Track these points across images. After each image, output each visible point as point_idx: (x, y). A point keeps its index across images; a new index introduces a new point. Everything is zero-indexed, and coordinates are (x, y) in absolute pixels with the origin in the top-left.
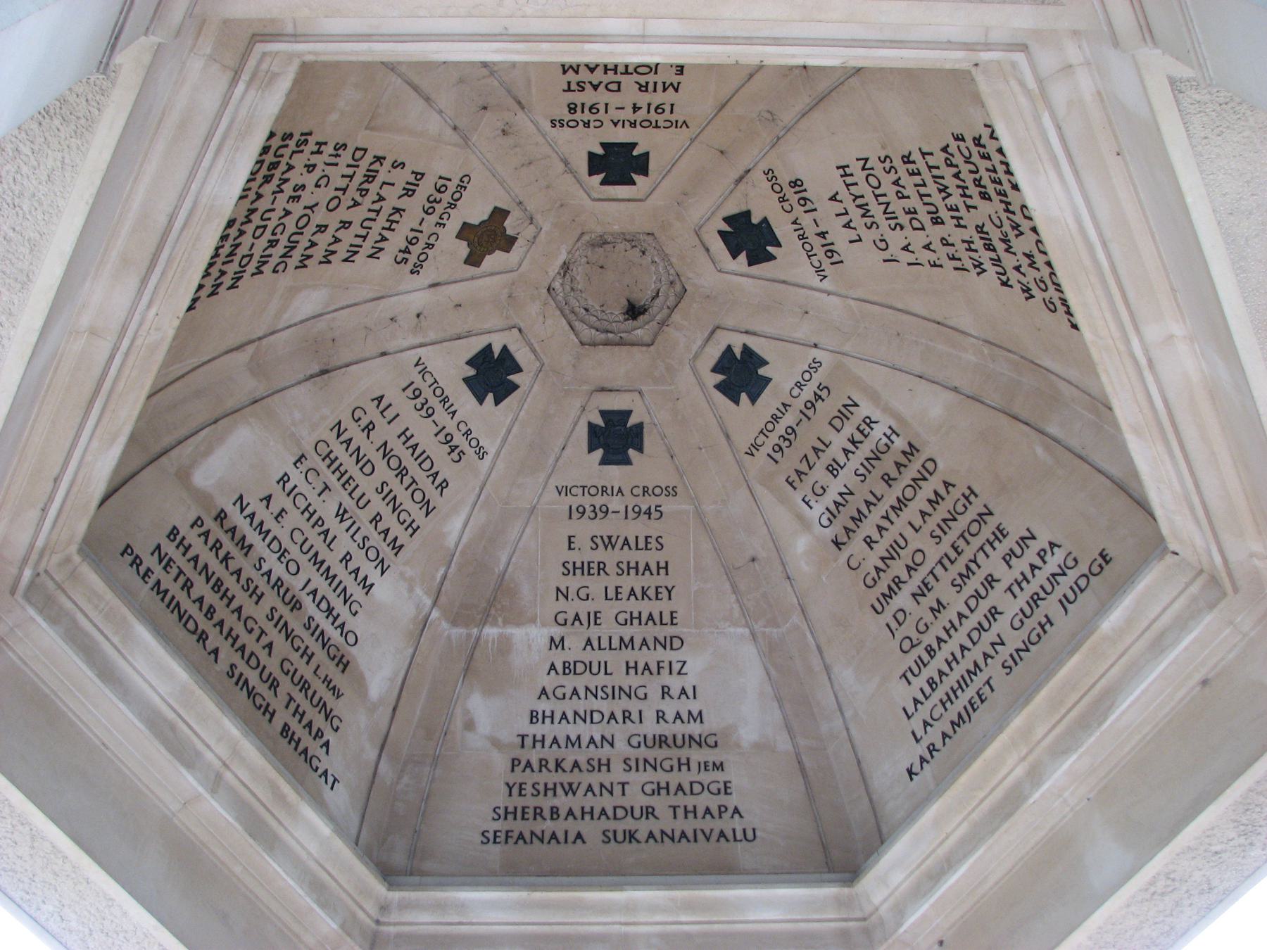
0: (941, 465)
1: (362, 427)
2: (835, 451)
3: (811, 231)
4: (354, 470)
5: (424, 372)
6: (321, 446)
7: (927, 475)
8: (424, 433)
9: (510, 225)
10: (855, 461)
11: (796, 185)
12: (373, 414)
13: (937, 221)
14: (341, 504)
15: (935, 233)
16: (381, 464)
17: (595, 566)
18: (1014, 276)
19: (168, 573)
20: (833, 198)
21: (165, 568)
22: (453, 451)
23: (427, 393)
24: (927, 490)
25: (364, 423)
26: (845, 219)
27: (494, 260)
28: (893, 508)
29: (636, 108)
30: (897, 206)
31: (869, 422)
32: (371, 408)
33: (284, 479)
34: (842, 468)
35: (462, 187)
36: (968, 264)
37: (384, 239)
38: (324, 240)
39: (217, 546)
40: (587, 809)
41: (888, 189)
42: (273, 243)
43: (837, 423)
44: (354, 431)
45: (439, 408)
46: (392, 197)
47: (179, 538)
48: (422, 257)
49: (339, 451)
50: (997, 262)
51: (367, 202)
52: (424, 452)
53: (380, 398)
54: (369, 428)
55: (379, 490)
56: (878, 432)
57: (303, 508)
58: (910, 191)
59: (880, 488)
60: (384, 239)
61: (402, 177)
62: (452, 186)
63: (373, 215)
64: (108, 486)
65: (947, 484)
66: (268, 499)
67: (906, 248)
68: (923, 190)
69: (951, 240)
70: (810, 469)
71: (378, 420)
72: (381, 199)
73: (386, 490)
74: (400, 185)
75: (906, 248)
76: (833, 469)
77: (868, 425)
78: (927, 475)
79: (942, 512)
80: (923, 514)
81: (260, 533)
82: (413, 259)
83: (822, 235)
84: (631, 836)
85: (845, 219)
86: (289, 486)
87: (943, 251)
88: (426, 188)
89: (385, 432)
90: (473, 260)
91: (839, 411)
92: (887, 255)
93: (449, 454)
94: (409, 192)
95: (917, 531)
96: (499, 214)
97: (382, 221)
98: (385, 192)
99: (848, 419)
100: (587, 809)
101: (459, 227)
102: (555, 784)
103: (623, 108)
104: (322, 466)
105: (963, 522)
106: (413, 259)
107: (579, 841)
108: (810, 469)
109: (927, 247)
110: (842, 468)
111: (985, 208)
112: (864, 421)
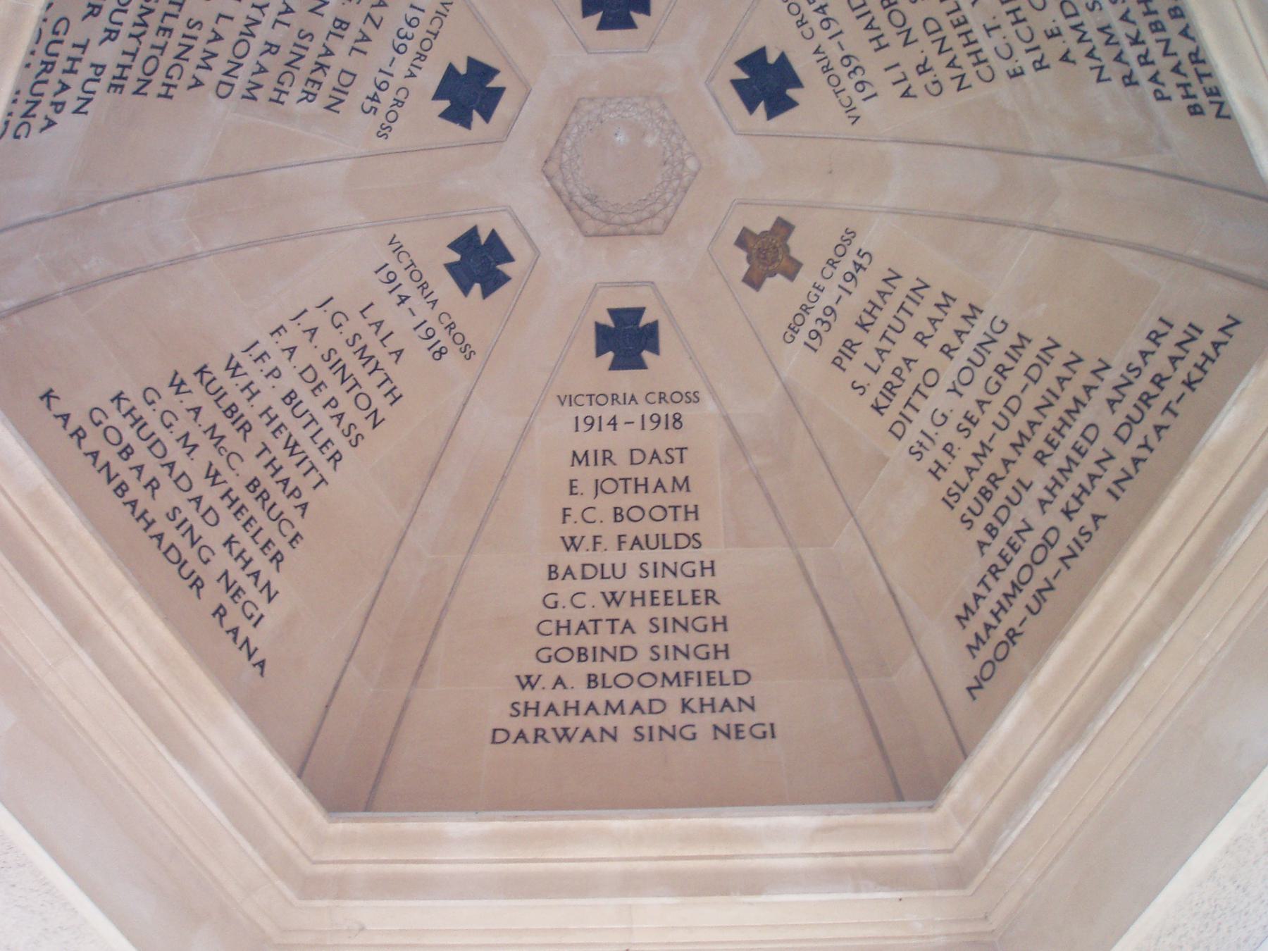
0: (212, 97)
1: (949, 458)
2: (341, 46)
3: (416, 301)
4: (952, 35)
5: (850, 108)
6: (988, 76)
7: (226, 79)
8: (856, 39)
9: (740, 263)
10: (315, 48)
11: (440, 352)
12: (917, 83)
13: (290, 398)
14: (211, 465)
15: (290, 380)
16: (915, 22)
17: (702, 594)
18: (199, 396)
19: (157, 34)
20: (399, 353)
21: (112, 85)
22: (372, 99)
23: (849, 84)
24: (219, 65)
25: (928, 77)
26: (384, 331)
27: (762, 223)
28: (257, 22)
29: (613, 423)
30: (334, 389)
31: (309, 96)
32: (917, 89)
33: (1040, 65)
34: (330, 33)
35: (793, 329)
36: (246, 362)
37: (882, 294)
38: (945, 335)
39: (1144, 60)
40: (572, 704)
41: (346, 404)
42: (1001, 370)
43: (346, 79)
44: (945, 74)
45: (835, 63)
46: (870, 341)
47: (259, 490)
48: (840, 250)
49: (965, 61)
50: (219, 395)
51: (894, 360)
52: (858, 17)
53: (905, 94)
54: (923, 69)
55: (326, 358)
56: (296, 92)
57: (554, 630)
58: (324, 416)
59: (279, 35)
60: (882, 294)
61: (855, 368)
62: (803, 336)
63: (891, 334)
64: (290, 771)
65: (198, 83)
66: (1065, 58)
67: (313, 331)
68: (313, 428)
69: (271, 380)
70: (369, 15)
71: (912, 74)
72: (880, 352)
73: (334, 358)
74: (859, 359)
75: (313, 331)
76: (341, 24)
77: (309, 93)
78: (226, 79)
79: (195, 56)
80: (218, 38)
81: (203, 59)
82: (852, 255)
83: (403, 299)
84: (540, 735)
85: (384, 331)
86: (1036, 55)
87: (277, 359)
88: (833, 342)
89: (910, 59)
90: (784, 227)
91: (346, 93)
92: (331, 307)
93: (368, 98)
94: (850, 346)
95: (220, 16)
96: (754, 281)
97: (885, 318)
98: (874, 361)
99: (334, 89)
100: (572, 704)
101: (800, 275)
102: (566, 714)
103: (626, 423)
104: (988, 53)
105: (167, 60)
106: (852, 255)
107: (627, 631)
108: (369, 15)
109: (292, 350)
110: (330, 33)
111: (253, 467)
112: (315, 95)
